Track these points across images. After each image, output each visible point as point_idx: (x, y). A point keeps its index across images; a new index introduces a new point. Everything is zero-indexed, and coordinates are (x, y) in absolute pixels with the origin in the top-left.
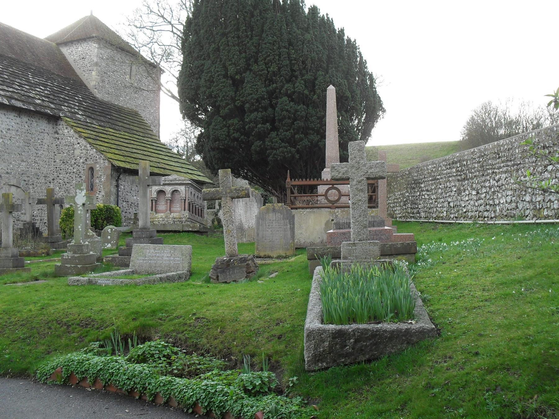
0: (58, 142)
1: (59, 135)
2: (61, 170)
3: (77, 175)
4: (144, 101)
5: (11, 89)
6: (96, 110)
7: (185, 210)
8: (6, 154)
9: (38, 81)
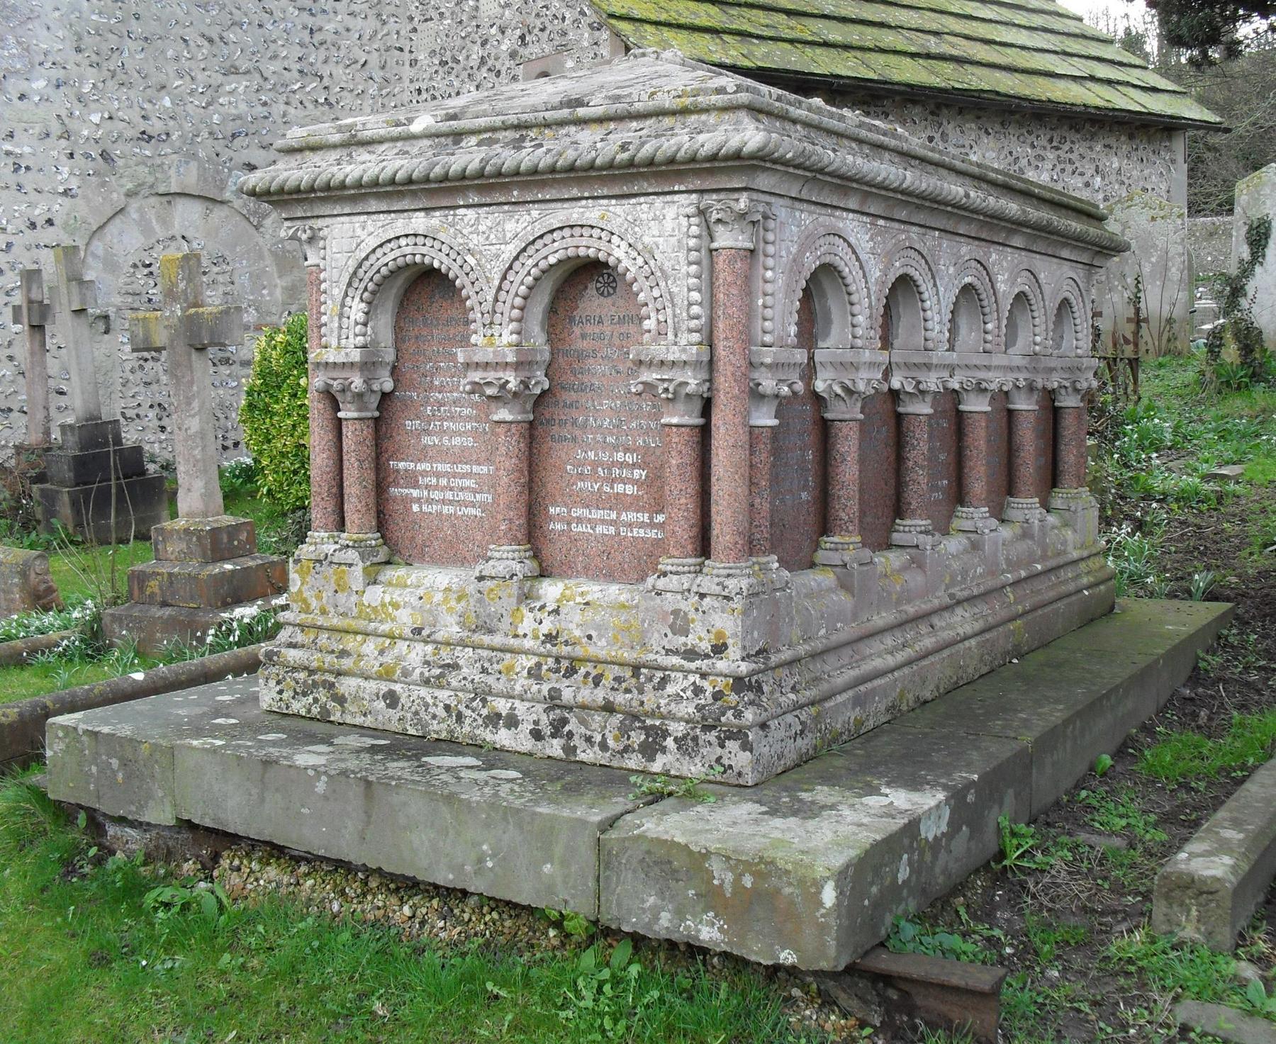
7: (704, 547)
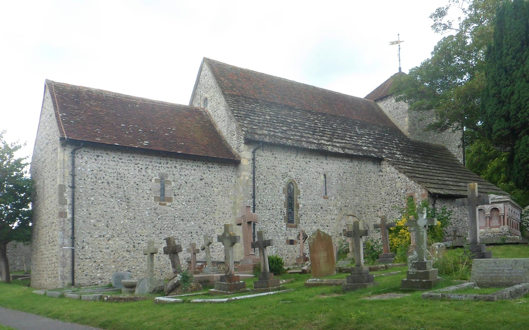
0: (382, 179)
2: (386, 200)
4: (450, 137)
5: (344, 141)
6: (410, 149)
7: (504, 225)
9: (363, 132)
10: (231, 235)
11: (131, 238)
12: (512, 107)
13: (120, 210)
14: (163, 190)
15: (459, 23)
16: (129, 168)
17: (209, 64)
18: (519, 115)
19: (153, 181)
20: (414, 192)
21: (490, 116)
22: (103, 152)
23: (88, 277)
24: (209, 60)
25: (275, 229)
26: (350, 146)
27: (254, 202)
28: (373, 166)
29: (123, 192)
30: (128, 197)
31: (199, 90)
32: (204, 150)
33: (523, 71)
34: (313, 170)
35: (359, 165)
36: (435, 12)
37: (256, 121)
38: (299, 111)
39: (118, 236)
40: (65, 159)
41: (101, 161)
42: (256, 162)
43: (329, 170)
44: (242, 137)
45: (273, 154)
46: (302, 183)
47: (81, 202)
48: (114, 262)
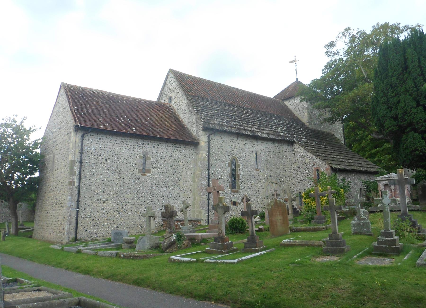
1: (295, 152)
2: (298, 172)
3: (308, 175)
5: (268, 129)
8: (269, 166)
10: (224, 205)
11: (120, 201)
12: (400, 111)
13: (113, 180)
14: (144, 164)
15: (344, 51)
16: (121, 148)
17: (174, 74)
18: (406, 117)
19: (138, 157)
20: (320, 167)
21: (382, 117)
22: (104, 136)
23: (87, 233)
24: (173, 70)
25: (223, 193)
26: (272, 132)
27: (209, 173)
28: (288, 147)
29: (116, 166)
30: (120, 169)
31: (165, 91)
32: (174, 135)
33: (405, 88)
34: (249, 150)
35: (279, 147)
36: (328, 44)
37: (209, 114)
38: (235, 107)
39: (111, 200)
40: (76, 141)
41: (102, 143)
42: (210, 144)
43: (259, 150)
44: (200, 125)
45: (221, 138)
46: (241, 159)
47: (86, 173)
48: (107, 220)
